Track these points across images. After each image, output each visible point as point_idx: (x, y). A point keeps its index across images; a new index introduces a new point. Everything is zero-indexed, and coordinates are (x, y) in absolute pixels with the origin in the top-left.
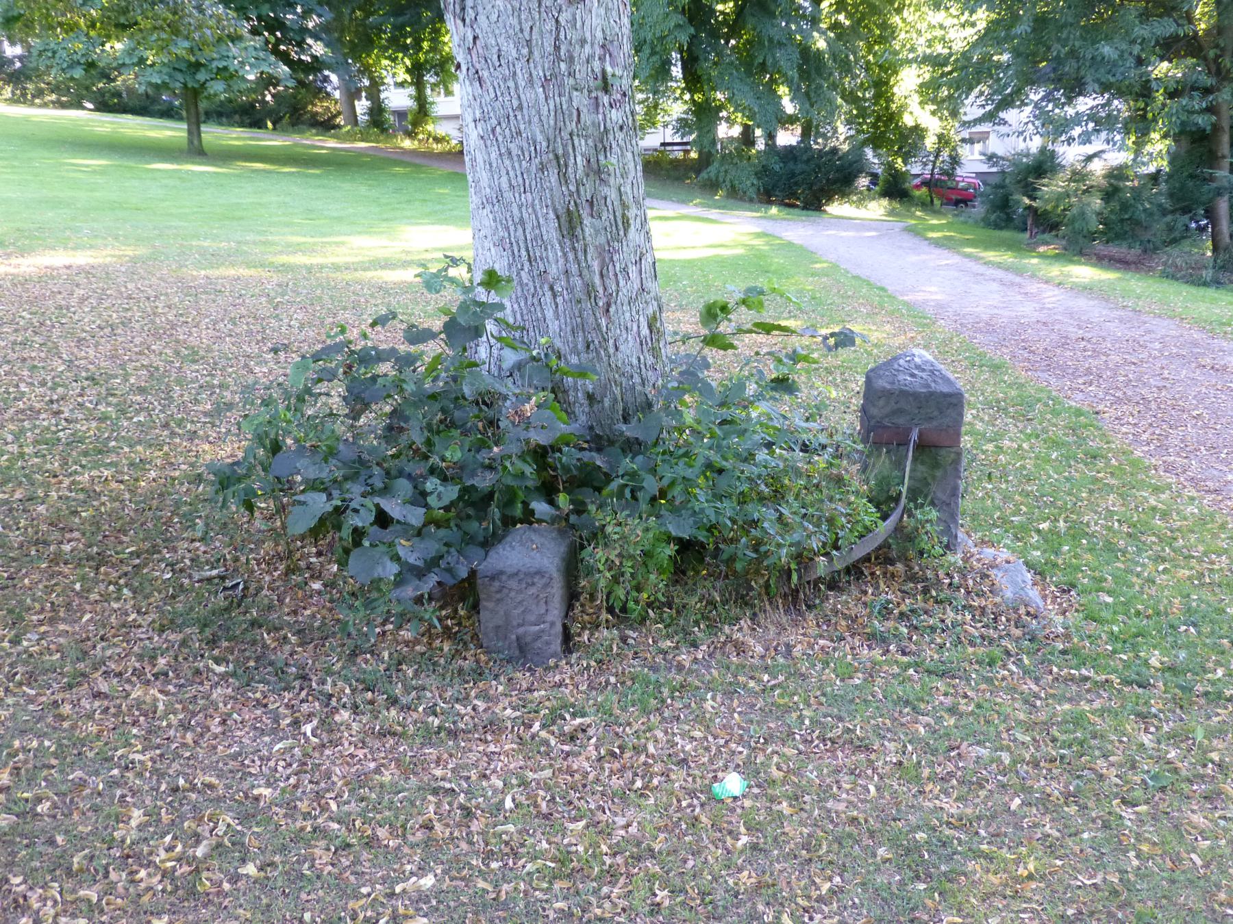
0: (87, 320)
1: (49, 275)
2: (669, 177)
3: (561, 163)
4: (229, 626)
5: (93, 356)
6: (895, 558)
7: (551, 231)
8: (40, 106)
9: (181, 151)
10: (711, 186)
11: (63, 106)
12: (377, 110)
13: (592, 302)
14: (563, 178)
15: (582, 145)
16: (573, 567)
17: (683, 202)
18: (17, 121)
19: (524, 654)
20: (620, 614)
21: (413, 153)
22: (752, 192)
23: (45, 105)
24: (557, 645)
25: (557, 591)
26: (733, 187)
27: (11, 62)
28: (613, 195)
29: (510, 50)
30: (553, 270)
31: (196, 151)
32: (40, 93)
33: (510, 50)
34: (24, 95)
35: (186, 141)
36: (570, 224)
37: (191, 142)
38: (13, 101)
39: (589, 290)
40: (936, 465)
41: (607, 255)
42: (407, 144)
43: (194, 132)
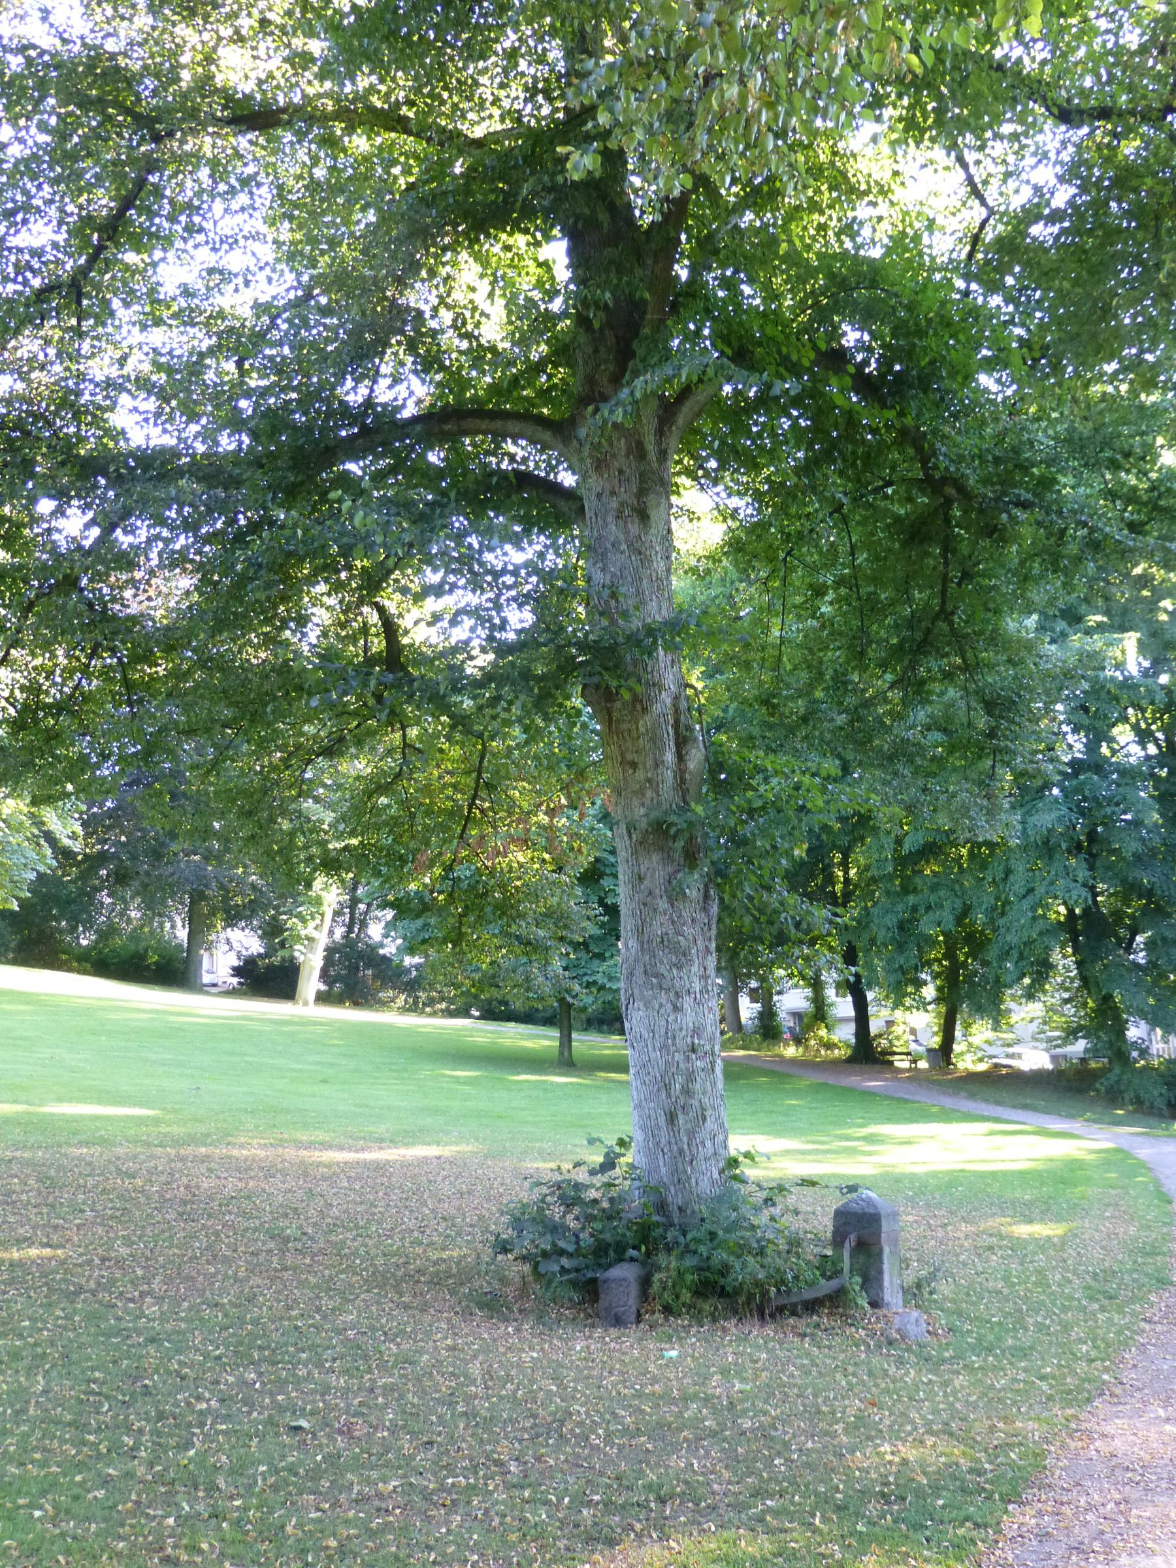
0: (447, 1189)
1: (425, 1160)
2: (1070, 1089)
3: (668, 1088)
4: (493, 1306)
5: (448, 1208)
6: (836, 1301)
7: (662, 1121)
8: (430, 1015)
9: (552, 1063)
10: (1113, 1097)
11: (451, 1014)
12: (768, 1015)
13: (682, 1159)
14: (669, 1095)
15: (679, 1079)
16: (645, 1282)
17: (1071, 1117)
18: (408, 1032)
19: (618, 1322)
20: (667, 1310)
21: (793, 1062)
22: (1160, 1103)
23: (434, 1014)
24: (633, 1318)
25: (634, 1290)
26: (1138, 1098)
27: (409, 971)
28: (695, 1103)
29: (645, 1034)
30: (663, 1141)
31: (566, 1062)
32: (431, 1002)
33: (645, 1034)
34: (416, 1003)
35: (556, 1052)
36: (672, 1118)
37: (561, 1053)
38: (405, 1010)
39: (681, 1152)
40: (869, 1255)
41: (691, 1135)
42: (791, 1051)
43: (566, 1041)
